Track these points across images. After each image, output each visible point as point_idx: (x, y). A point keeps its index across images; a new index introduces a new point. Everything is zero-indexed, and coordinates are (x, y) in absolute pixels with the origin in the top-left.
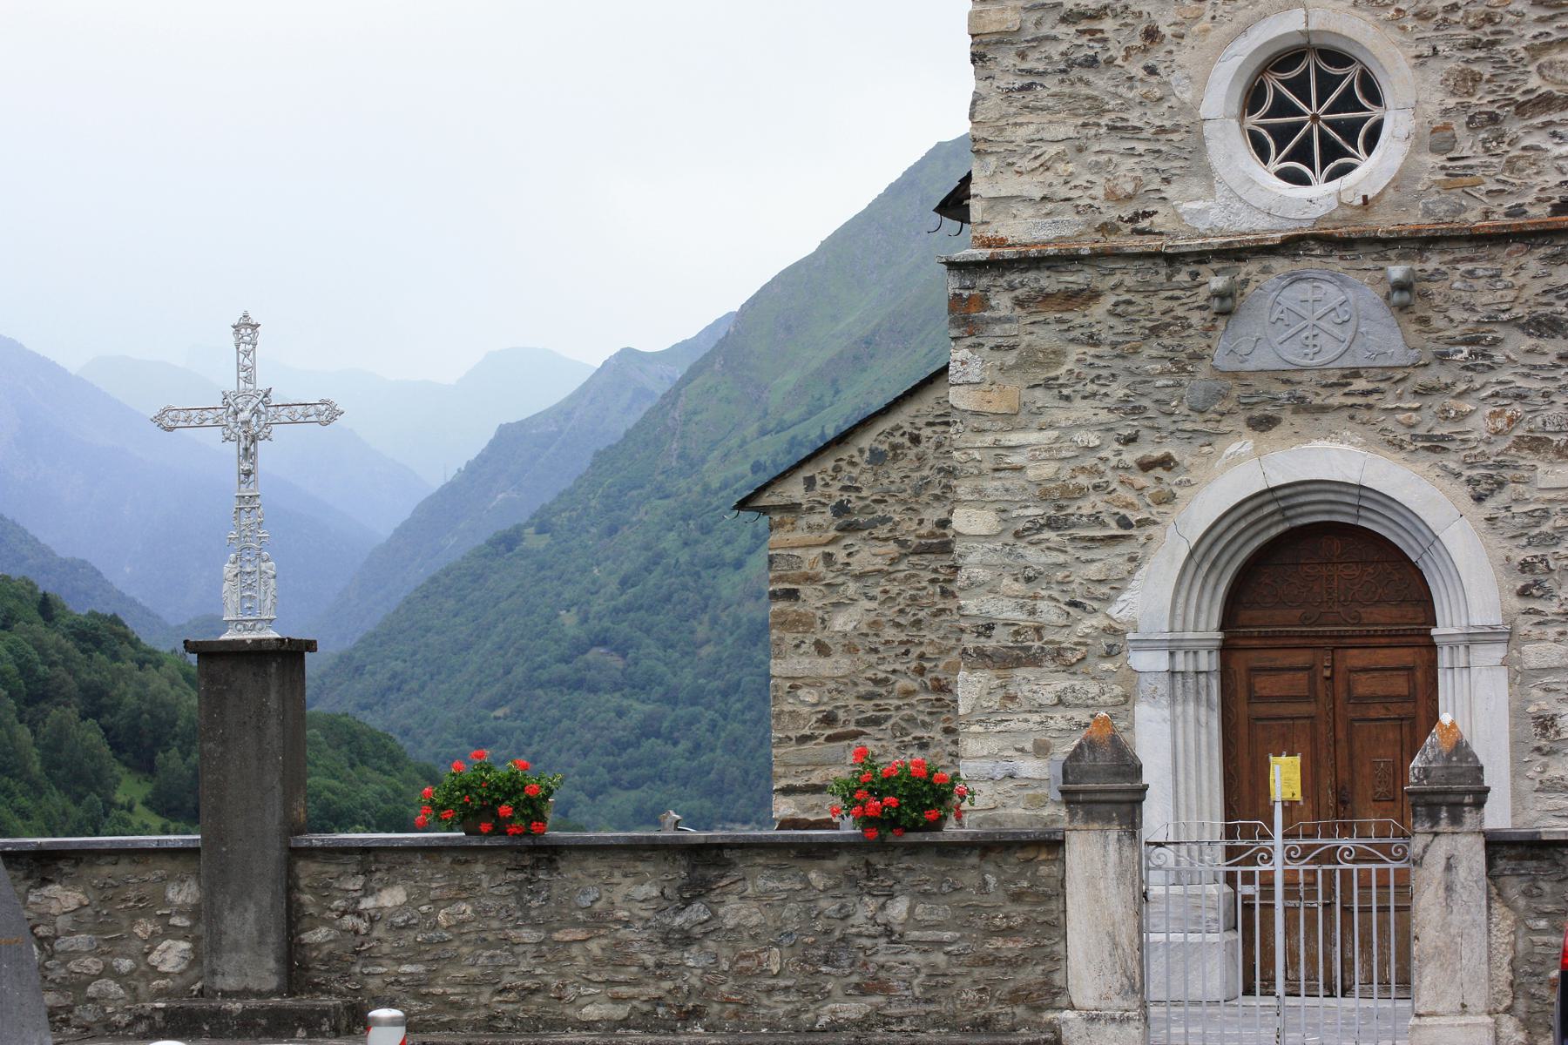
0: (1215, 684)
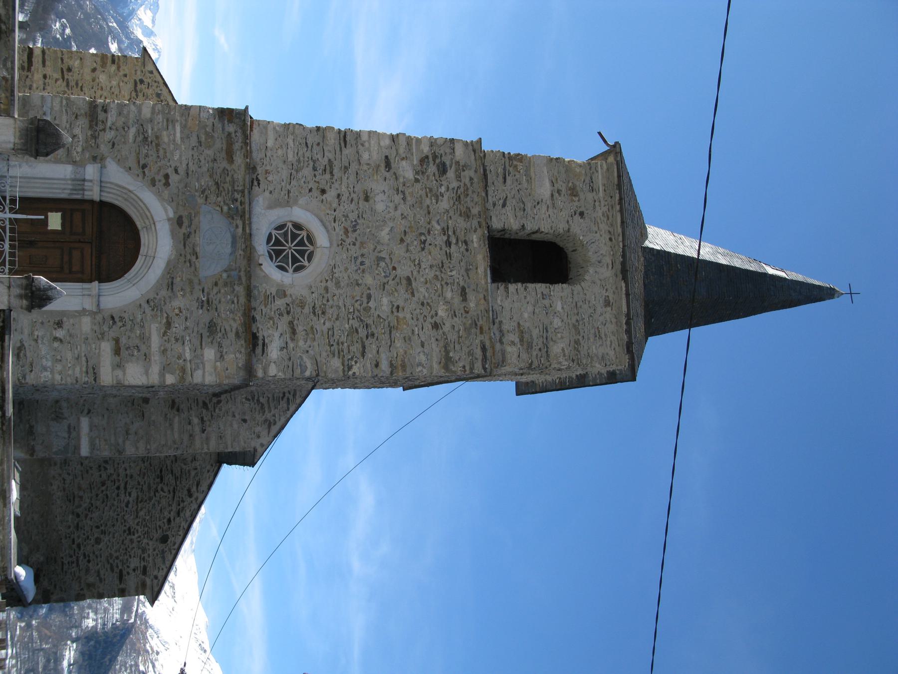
0: (79, 197)
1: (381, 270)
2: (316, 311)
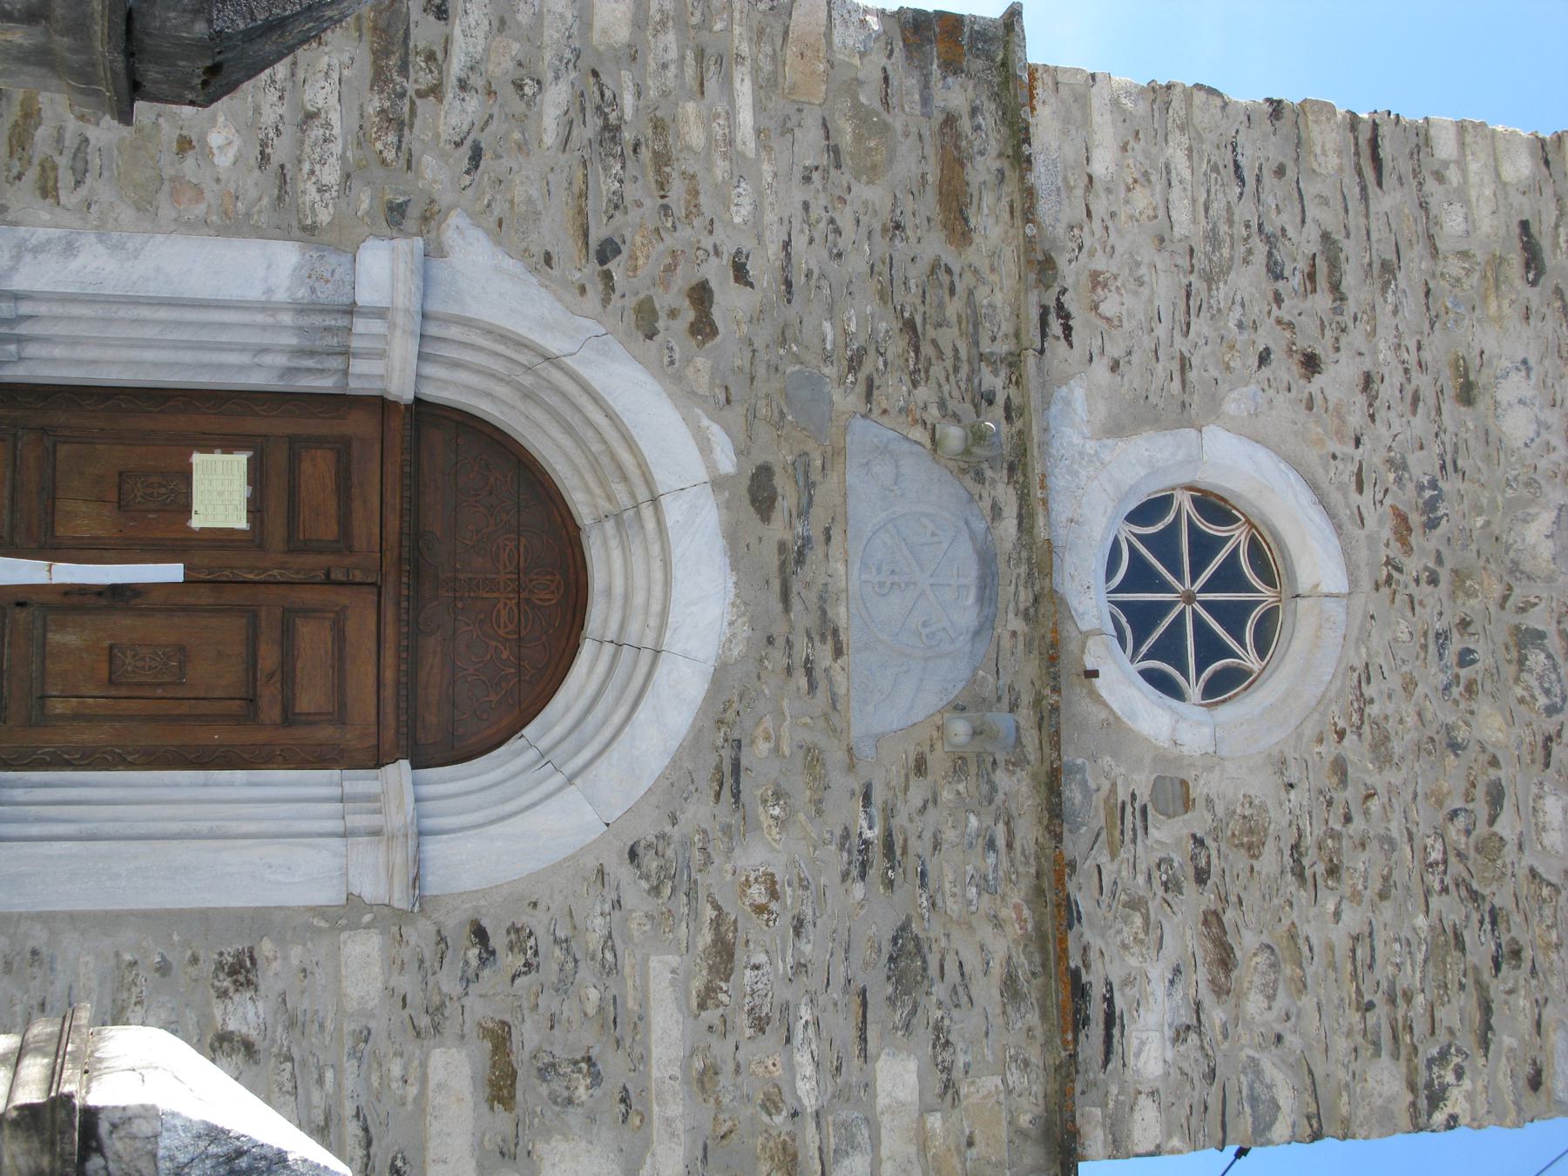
0: (325, 384)
1: (1534, 683)
2: (1306, 862)
